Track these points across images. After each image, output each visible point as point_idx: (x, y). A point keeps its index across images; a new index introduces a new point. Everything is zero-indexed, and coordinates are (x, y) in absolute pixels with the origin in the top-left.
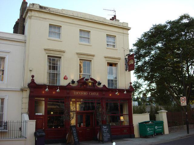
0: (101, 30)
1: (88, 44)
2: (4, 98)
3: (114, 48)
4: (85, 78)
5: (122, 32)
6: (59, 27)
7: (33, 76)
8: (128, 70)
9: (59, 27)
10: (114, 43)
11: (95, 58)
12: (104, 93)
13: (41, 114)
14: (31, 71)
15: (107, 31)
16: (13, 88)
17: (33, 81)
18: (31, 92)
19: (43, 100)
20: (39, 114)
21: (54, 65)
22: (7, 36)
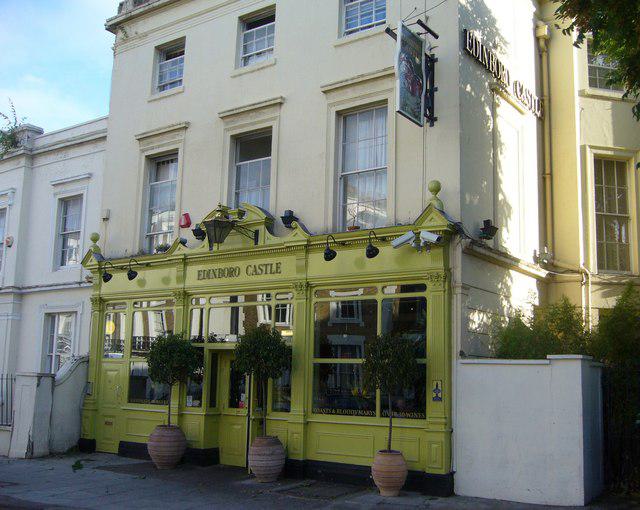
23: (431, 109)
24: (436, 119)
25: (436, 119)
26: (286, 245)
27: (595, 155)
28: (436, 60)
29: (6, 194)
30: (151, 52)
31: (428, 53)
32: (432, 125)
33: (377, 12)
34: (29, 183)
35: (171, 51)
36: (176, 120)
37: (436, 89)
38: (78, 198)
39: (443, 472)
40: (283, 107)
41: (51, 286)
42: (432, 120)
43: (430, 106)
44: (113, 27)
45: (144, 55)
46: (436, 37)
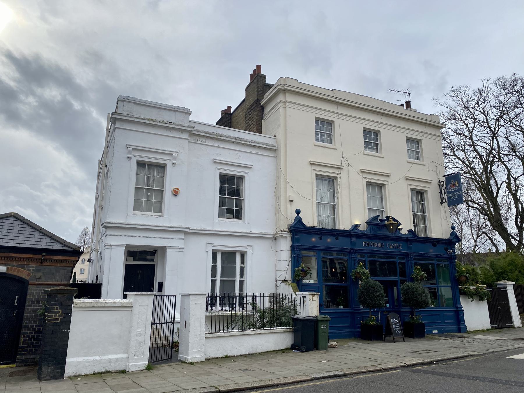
0: (305, 108)
1: (374, 153)
2: (247, 251)
3: (417, 161)
4: (380, 218)
5: (379, 120)
6: (330, 123)
7: (298, 212)
8: (446, 204)
9: (330, 123)
10: (231, 121)
11: (390, 180)
12: (410, 245)
13: (312, 281)
14: (291, 201)
15: (315, 111)
16: (264, 232)
17: (299, 220)
18: (293, 240)
19: (312, 256)
20: (308, 281)
21: (154, 186)
22: (208, 129)
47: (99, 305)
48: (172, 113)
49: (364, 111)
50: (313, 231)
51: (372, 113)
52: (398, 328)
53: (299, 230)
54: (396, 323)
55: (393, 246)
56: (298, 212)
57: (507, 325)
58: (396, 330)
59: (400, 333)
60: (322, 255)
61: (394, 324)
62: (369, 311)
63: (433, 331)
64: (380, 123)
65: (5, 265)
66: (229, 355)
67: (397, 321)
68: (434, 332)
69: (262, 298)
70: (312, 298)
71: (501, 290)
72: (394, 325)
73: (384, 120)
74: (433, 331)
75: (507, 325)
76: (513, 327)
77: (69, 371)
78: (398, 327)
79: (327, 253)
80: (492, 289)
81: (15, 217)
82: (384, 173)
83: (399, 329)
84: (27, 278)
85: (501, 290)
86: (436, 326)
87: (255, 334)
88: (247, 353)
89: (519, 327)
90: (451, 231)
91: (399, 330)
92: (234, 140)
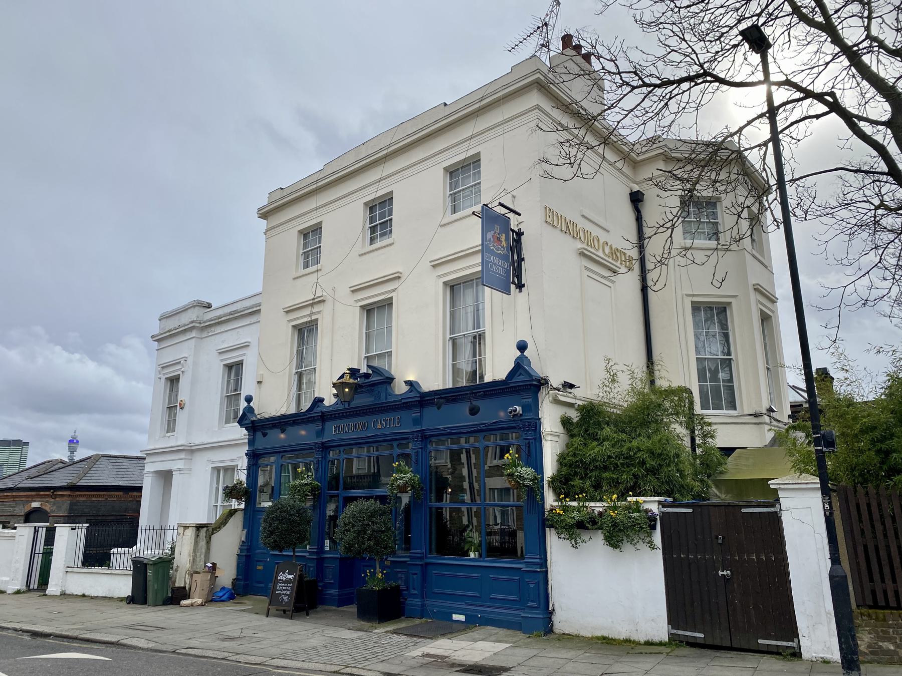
7: (522, 347)
23: (519, 277)
24: (523, 286)
25: (523, 286)
26: (403, 401)
27: (692, 302)
28: (523, 234)
29: (180, 362)
30: (297, 232)
31: (516, 229)
32: (520, 291)
33: (463, 198)
34: (883, 173)
35: (312, 234)
36: (389, 271)
37: (523, 259)
38: (240, 364)
39: (183, 586)
40: (326, 302)
41: (232, 441)
42: (520, 286)
43: (518, 273)
44: (265, 214)
45: (290, 240)
46: (519, 215)
47: (6, 535)
48: (177, 317)
49: (290, 206)
50: (282, 422)
51: (295, 203)
52: (288, 590)
53: (525, 385)
54: (288, 581)
55: (383, 422)
56: (522, 347)
57: (760, 641)
58: (280, 594)
59: (286, 601)
60: (373, 453)
61: (280, 583)
62: (292, 554)
63: (454, 615)
64: (317, 209)
65: (39, 501)
66: (86, 594)
67: (291, 577)
68: (456, 617)
69: (147, 531)
70: (184, 531)
71: (744, 510)
72: (280, 585)
73: (311, 204)
74: (454, 615)
75: (760, 641)
76: (796, 654)
77: (47, 592)
78: (290, 588)
79: (392, 446)
80: (690, 510)
81: (61, 462)
82: (384, 277)
83: (288, 593)
84: (49, 511)
85: (744, 510)
86: (467, 604)
87: (111, 574)
88: (104, 595)
89: (826, 662)
90: (519, 353)
91: (287, 595)
92: (231, 316)
